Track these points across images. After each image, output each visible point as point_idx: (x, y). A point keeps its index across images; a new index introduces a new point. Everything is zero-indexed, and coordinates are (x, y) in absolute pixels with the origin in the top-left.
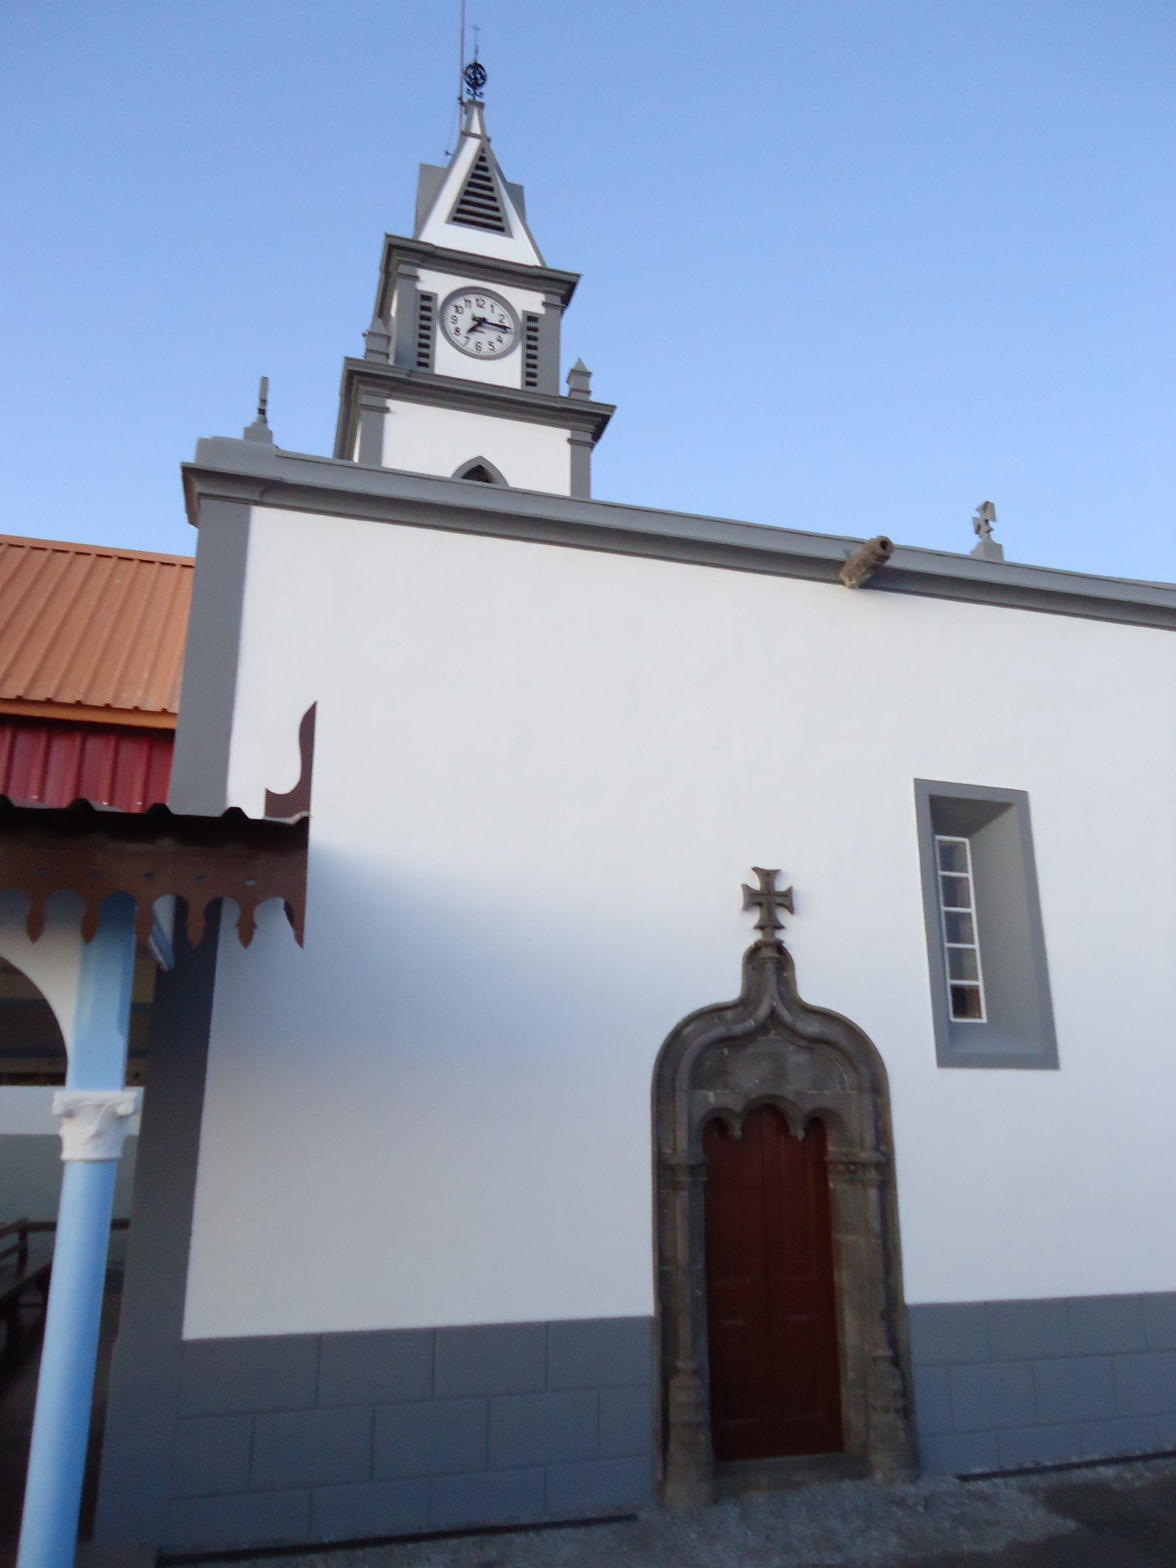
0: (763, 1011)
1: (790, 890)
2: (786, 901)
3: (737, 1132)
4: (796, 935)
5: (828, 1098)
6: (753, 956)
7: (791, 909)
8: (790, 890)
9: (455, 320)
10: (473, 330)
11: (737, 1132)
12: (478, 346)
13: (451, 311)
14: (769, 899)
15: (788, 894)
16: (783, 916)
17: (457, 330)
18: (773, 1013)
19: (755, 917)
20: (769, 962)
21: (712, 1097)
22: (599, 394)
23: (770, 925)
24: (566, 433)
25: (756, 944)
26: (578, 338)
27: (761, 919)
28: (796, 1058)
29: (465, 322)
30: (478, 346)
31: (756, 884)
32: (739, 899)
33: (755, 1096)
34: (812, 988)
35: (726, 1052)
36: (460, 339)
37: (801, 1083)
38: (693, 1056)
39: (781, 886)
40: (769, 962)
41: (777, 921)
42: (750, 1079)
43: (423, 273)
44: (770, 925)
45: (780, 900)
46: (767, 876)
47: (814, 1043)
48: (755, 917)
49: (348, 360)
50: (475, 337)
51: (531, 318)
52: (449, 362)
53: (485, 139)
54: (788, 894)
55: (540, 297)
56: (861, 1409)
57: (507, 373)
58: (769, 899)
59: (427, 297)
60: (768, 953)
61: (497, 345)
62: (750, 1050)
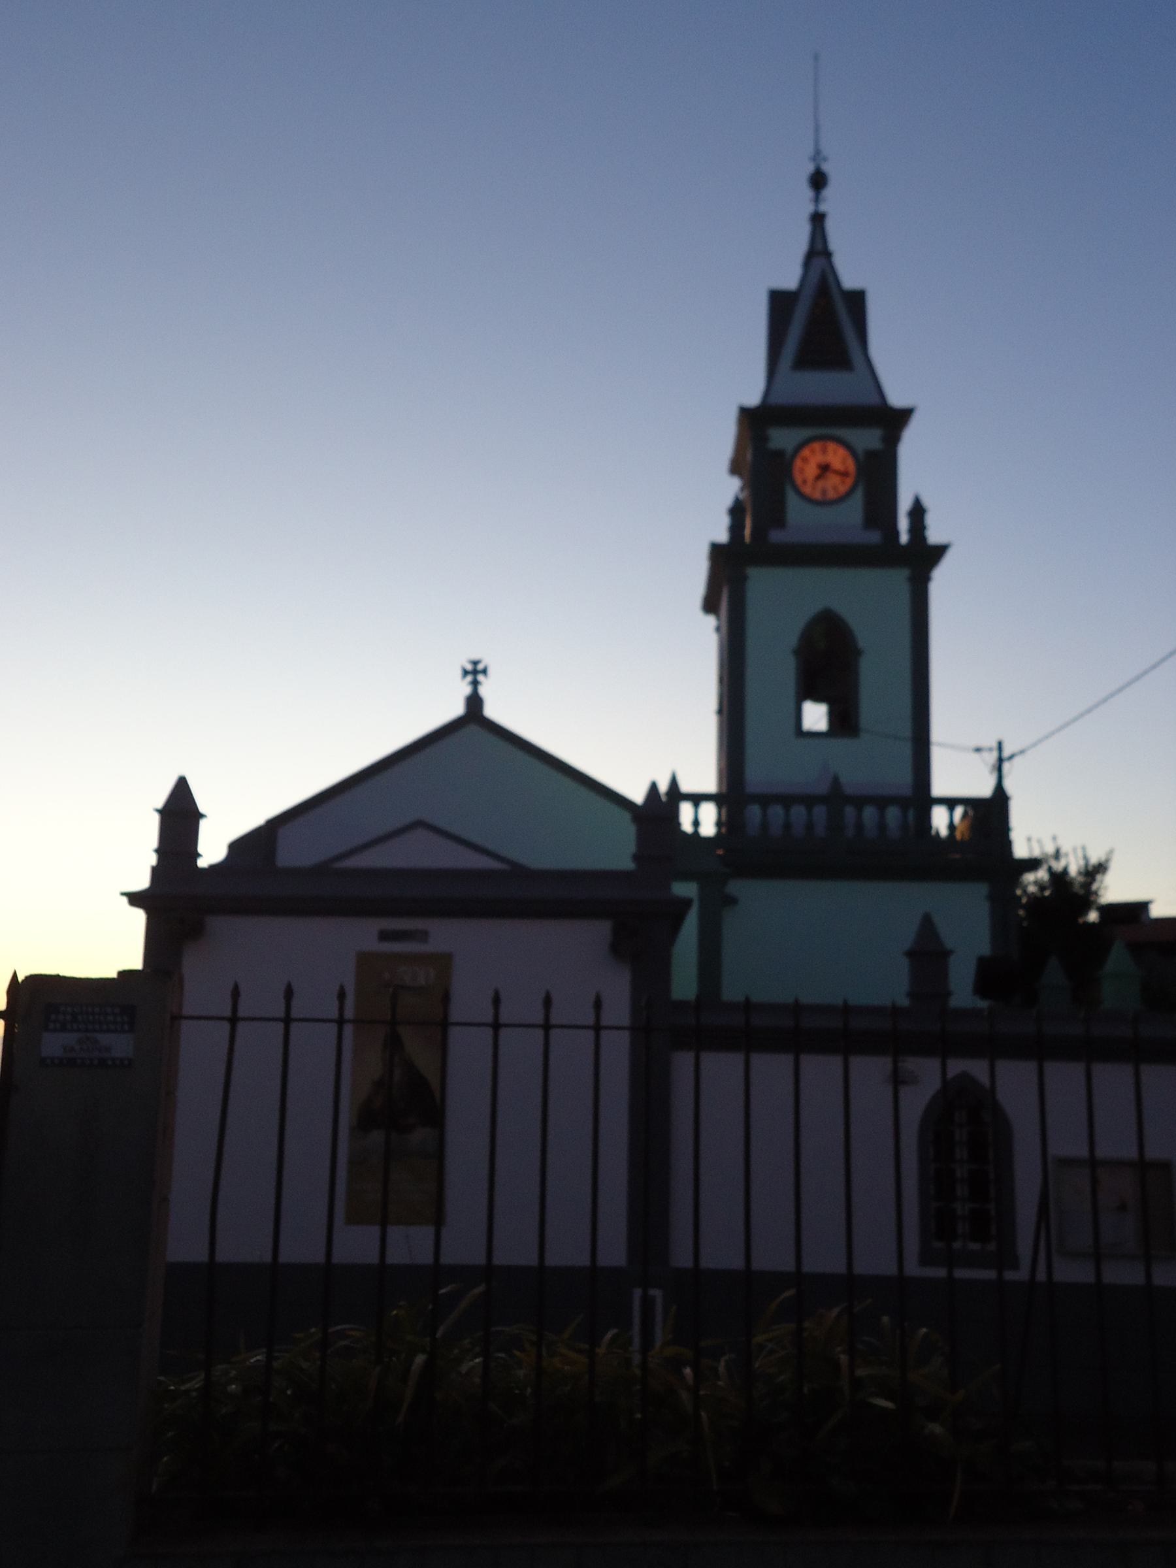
9: (802, 471)
10: (818, 478)
12: (824, 492)
17: (805, 482)
20: (474, 702)
23: (475, 684)
26: (917, 473)
29: (811, 470)
30: (824, 492)
36: (807, 490)
40: (474, 702)
44: (475, 684)
46: (475, 663)
50: (820, 484)
51: (871, 455)
52: (801, 521)
53: (827, 254)
57: (847, 521)
59: (780, 454)
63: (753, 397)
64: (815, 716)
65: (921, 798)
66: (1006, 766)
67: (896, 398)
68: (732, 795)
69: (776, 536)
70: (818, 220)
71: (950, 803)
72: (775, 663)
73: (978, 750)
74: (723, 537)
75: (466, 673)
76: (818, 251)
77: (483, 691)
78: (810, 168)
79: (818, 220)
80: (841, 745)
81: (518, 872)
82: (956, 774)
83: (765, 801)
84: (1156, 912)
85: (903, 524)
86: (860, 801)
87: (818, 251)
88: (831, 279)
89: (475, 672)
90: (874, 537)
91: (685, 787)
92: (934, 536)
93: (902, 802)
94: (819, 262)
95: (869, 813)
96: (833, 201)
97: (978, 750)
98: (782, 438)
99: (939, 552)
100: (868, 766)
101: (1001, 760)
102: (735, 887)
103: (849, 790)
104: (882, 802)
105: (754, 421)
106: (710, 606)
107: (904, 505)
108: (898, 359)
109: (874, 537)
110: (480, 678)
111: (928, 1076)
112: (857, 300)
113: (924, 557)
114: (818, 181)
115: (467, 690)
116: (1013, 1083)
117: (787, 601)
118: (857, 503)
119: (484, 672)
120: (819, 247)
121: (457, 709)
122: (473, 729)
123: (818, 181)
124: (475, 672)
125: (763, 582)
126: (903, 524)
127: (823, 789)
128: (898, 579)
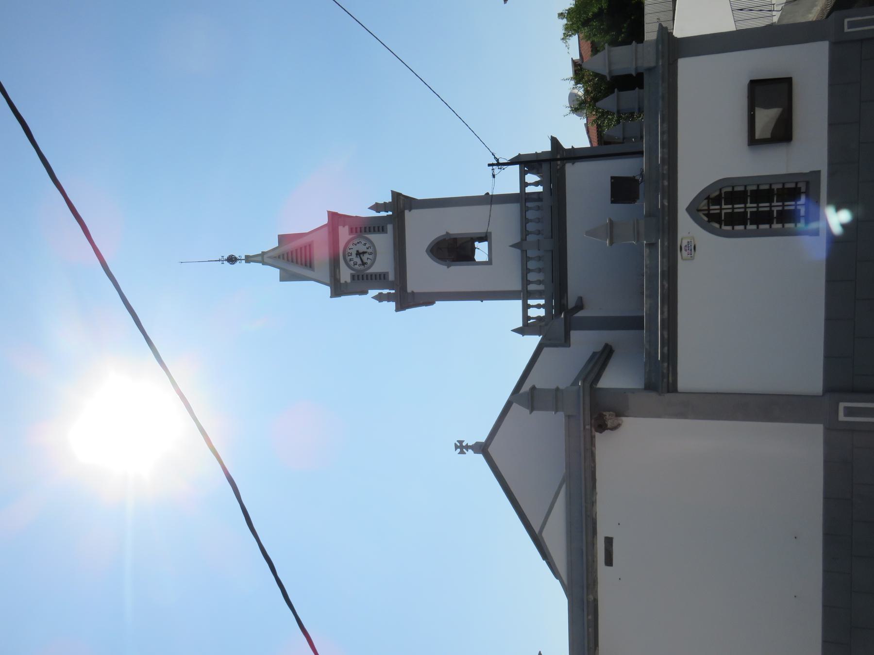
13: (357, 267)
22: (388, 199)
24: (407, 212)
43: (342, 281)
44: (468, 447)
46: (456, 447)
49: (612, 178)
52: (383, 263)
55: (341, 228)
57: (383, 242)
61: (367, 245)
63: (327, 290)
64: (481, 252)
65: (522, 198)
66: (501, 161)
67: (324, 220)
68: (524, 295)
69: (391, 277)
70: (248, 259)
71: (524, 184)
72: (457, 275)
73: (494, 176)
74: (392, 305)
75: (462, 452)
76: (262, 258)
77: (471, 443)
78: (226, 262)
79: (248, 259)
80: (494, 237)
81: (568, 479)
82: (509, 182)
83: (526, 282)
84: (577, 57)
85: (383, 214)
86: (525, 233)
87: (262, 258)
88: (272, 254)
89: (461, 447)
90: (390, 227)
91: (520, 324)
92: (388, 199)
93: (524, 211)
94: (266, 260)
95: (531, 227)
96: (240, 253)
97: (494, 176)
98: (345, 275)
99: (396, 196)
100: (505, 224)
101: (498, 164)
102: (571, 302)
103: (517, 239)
104: (524, 221)
105: (338, 290)
106: (431, 303)
107: (374, 214)
108: (308, 219)
109: (390, 227)
110: (464, 444)
111: (687, 228)
112: (282, 238)
113: (401, 204)
114: (232, 260)
115: (470, 451)
116: (691, 183)
117: (423, 270)
118: (373, 237)
119: (461, 442)
120: (260, 258)
121: (480, 457)
122: (491, 450)
123: (232, 260)
124: (461, 447)
125: (413, 286)
126: (383, 214)
127: (518, 252)
128: (410, 217)
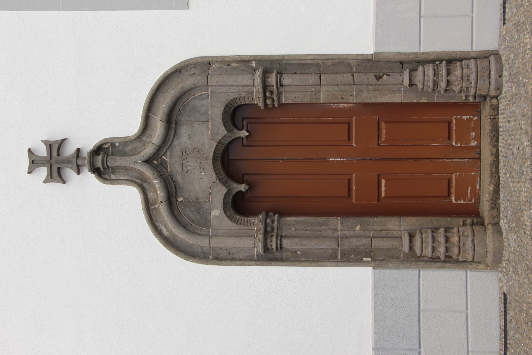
0: (147, 172)
1: (45, 142)
2: (56, 147)
3: (242, 188)
4: (85, 139)
5: (216, 112)
6: (100, 173)
7: (62, 143)
8: (45, 142)
11: (242, 188)
14: (54, 161)
15: (50, 145)
16: (69, 150)
18: (148, 161)
19: (70, 173)
20: (104, 161)
21: (216, 212)
23: (77, 161)
25: (94, 172)
27: (72, 168)
28: (185, 137)
31: (43, 172)
32: (56, 186)
33: (159, 97)
34: (126, 123)
35: (180, 199)
37: (204, 134)
38: (177, 222)
39: (42, 151)
40: (104, 161)
41: (72, 155)
42: (203, 183)
44: (77, 161)
45: (55, 153)
46: (34, 163)
47: (171, 122)
48: (70, 173)
54: (50, 145)
56: (464, 84)
58: (54, 161)
60: (99, 161)
62: (179, 178)
